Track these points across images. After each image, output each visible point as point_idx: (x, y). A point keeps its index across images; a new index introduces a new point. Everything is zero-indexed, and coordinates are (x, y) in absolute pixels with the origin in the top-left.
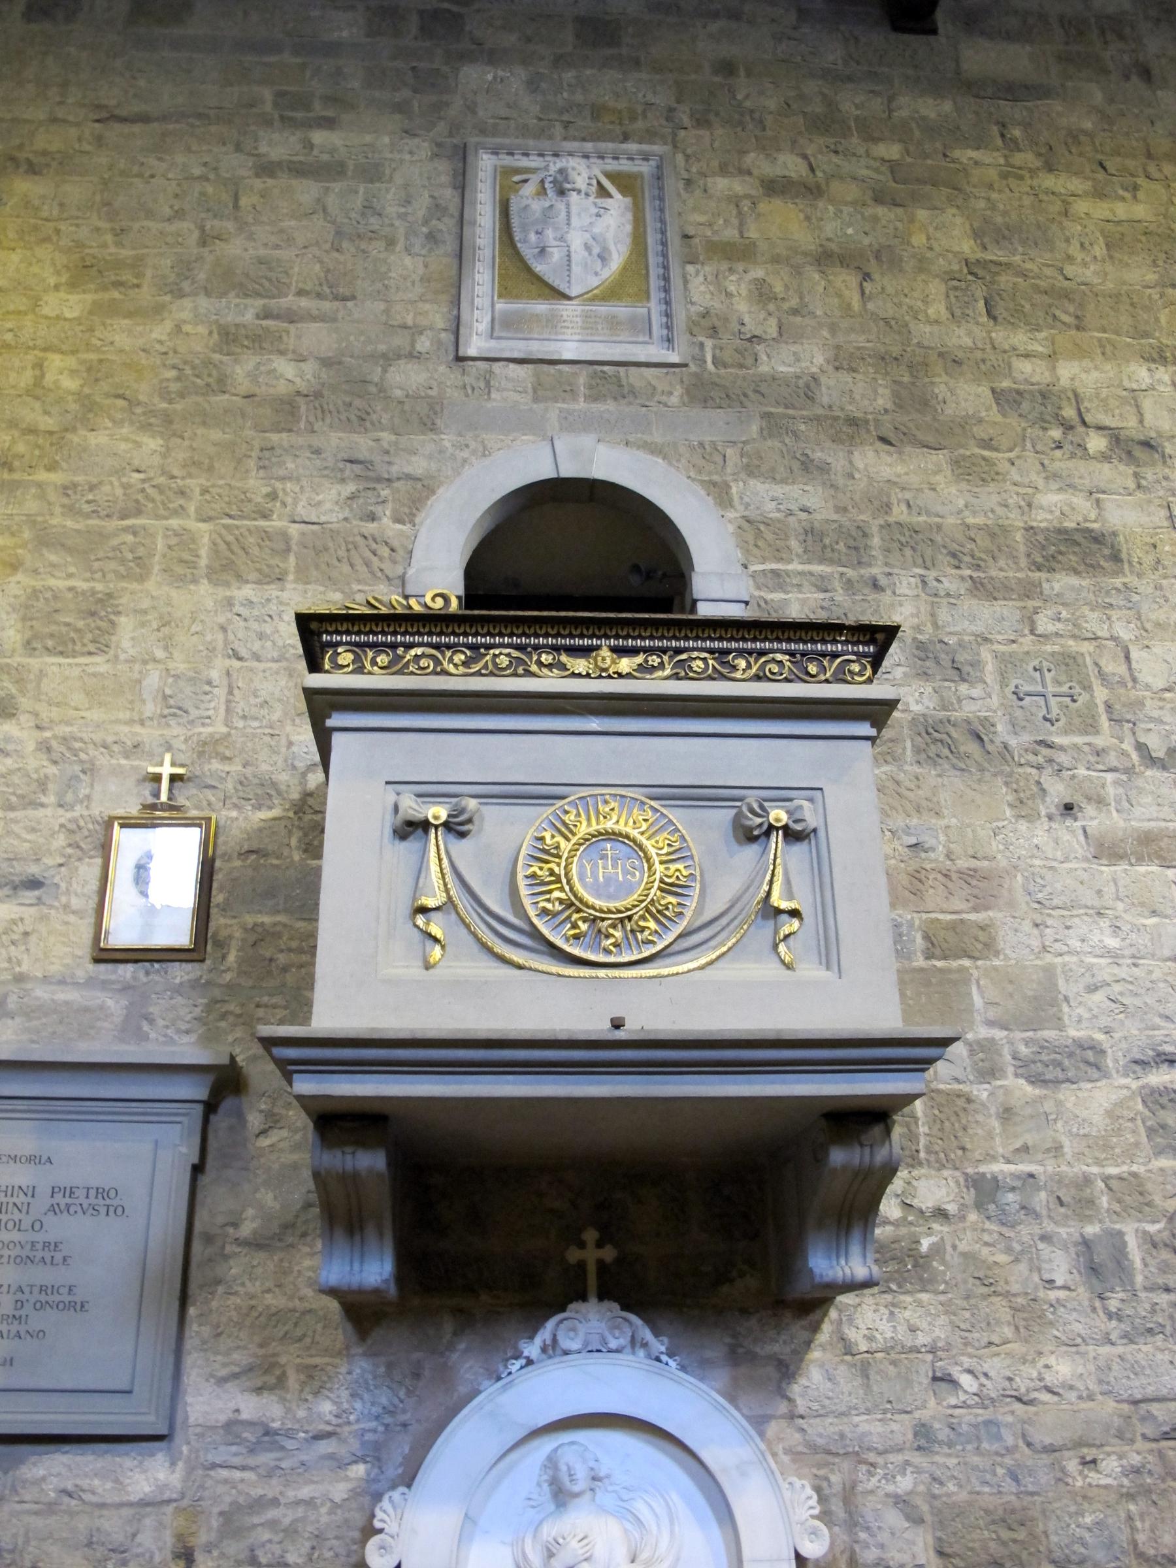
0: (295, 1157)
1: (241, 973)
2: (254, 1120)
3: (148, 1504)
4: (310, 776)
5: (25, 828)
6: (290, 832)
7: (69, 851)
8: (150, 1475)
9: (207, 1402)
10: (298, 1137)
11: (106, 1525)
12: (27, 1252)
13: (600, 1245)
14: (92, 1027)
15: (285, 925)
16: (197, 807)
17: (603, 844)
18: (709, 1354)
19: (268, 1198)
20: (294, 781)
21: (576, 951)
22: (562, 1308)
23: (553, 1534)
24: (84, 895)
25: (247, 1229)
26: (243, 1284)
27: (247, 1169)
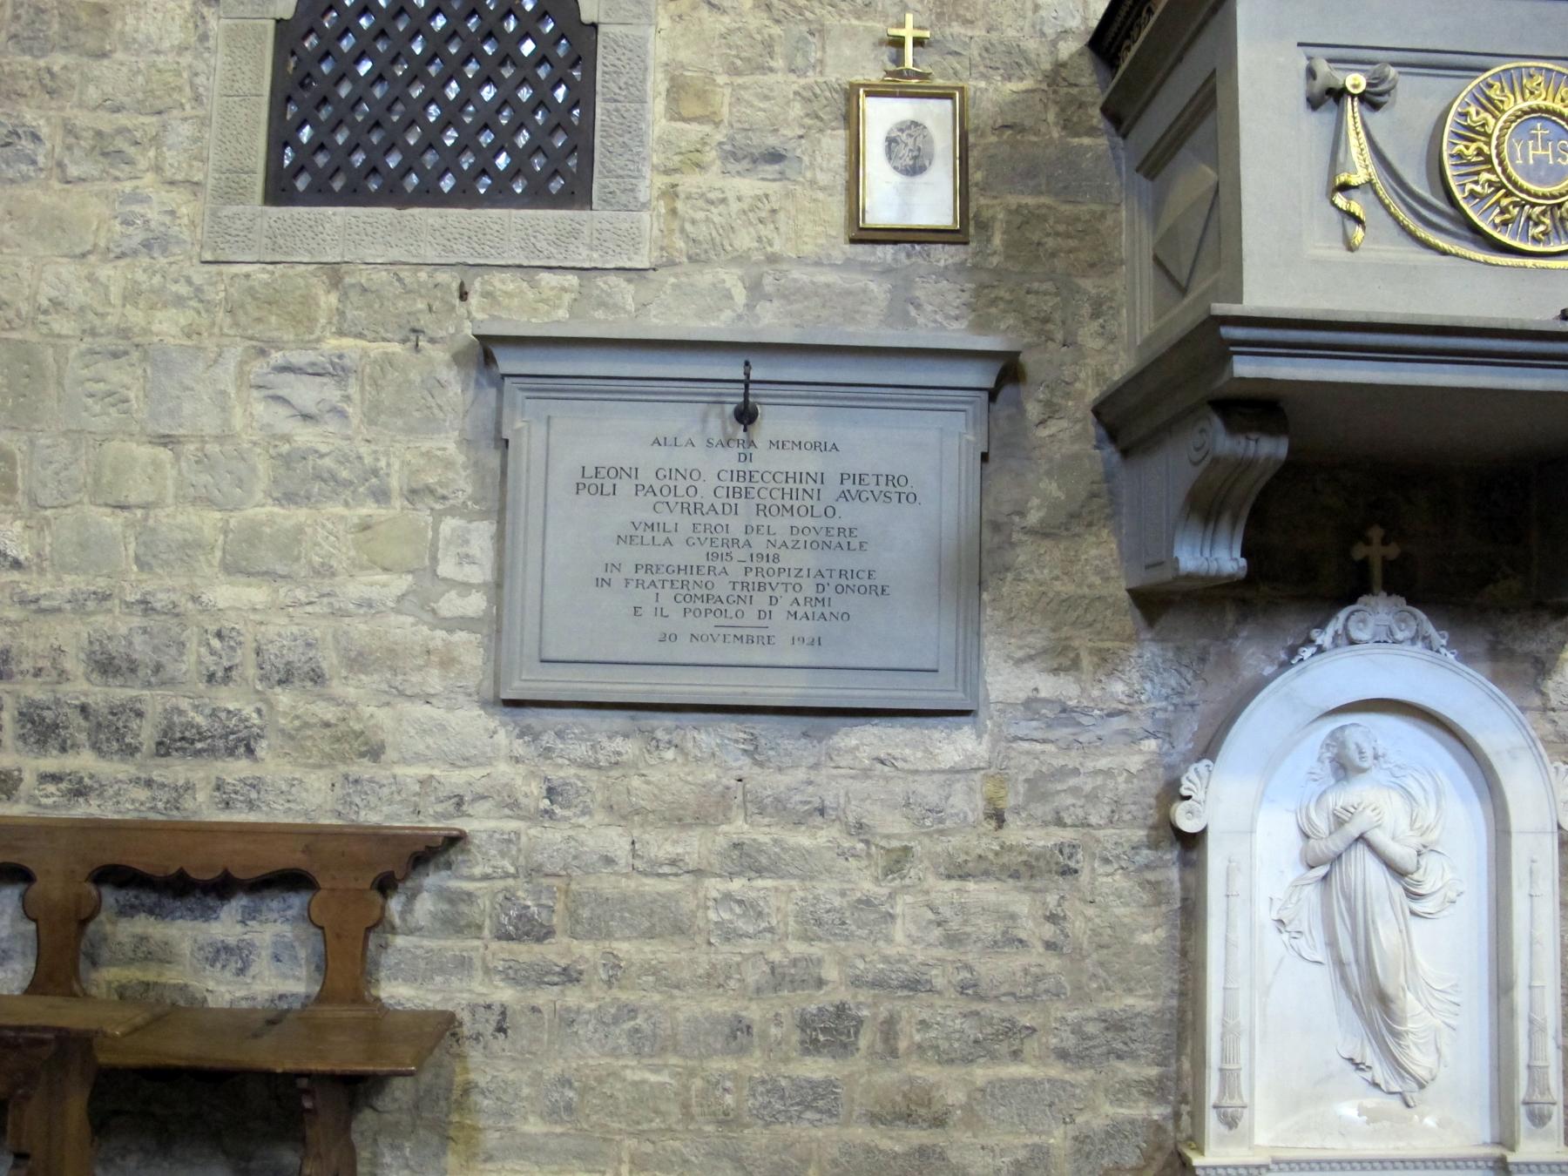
0: (1076, 447)
1: (1008, 257)
2: (1033, 410)
3: (958, 772)
4: (1062, 45)
5: (757, 95)
6: (1046, 106)
7: (808, 121)
8: (957, 746)
9: (1006, 681)
10: (1078, 427)
11: (922, 790)
12: (822, 537)
13: (1385, 542)
14: (858, 312)
15: (1049, 208)
16: (942, 76)
17: (1533, 123)
18: (1471, 649)
19: (1052, 488)
20: (1044, 50)
21: (1505, 238)
22: (1352, 601)
23: (1340, 803)
24: (830, 170)
25: (1034, 518)
26: (1031, 572)
27: (1029, 458)
